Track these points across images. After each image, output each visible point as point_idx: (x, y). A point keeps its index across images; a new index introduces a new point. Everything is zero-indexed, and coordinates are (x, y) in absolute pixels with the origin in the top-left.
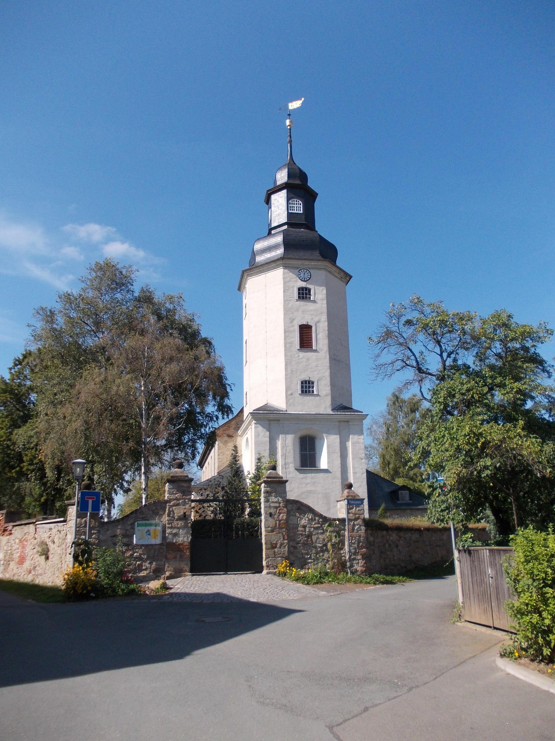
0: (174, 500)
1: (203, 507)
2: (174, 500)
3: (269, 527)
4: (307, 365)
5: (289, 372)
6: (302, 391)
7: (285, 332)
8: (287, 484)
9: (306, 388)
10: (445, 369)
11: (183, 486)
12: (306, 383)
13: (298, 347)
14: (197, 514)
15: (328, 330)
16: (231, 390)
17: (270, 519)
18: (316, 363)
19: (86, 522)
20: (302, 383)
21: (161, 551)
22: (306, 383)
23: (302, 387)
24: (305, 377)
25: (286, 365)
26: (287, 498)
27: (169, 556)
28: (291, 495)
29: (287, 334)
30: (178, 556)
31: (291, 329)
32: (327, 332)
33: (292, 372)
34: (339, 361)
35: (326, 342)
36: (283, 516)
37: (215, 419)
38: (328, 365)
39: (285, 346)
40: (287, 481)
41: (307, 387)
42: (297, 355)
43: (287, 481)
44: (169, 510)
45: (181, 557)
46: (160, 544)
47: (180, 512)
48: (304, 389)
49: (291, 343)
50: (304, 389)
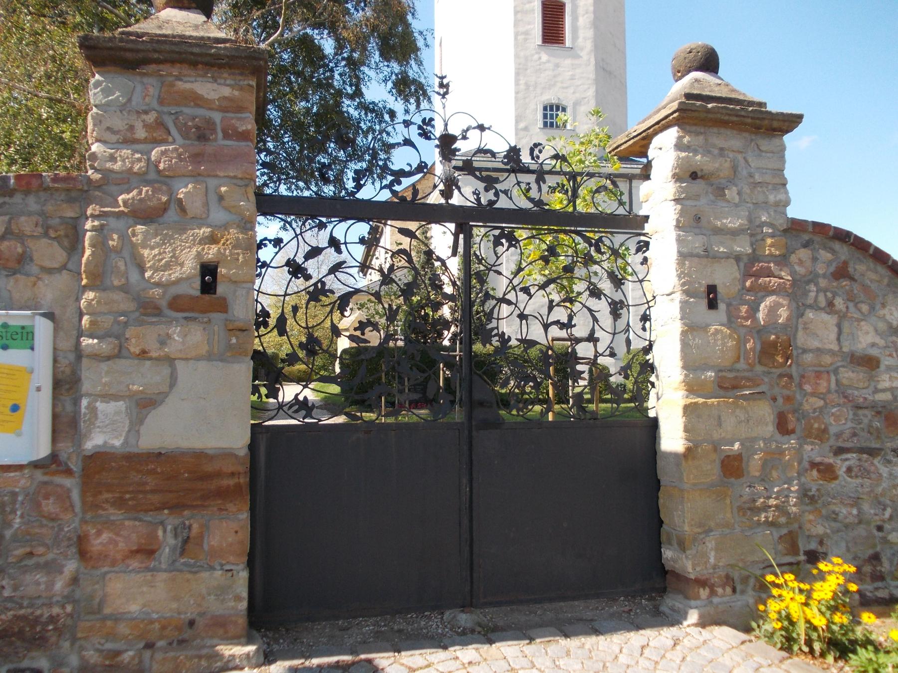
0: (142, 178)
1: (334, 243)
2: (142, 178)
3: (706, 367)
4: (555, 76)
5: (522, 87)
6: (545, 124)
7: (516, 13)
8: (794, 142)
9: (552, 117)
10: (30, 598)
11: (197, 100)
12: (552, 110)
13: (539, 41)
14: (299, 284)
15: (595, 12)
16: (427, 46)
17: (716, 323)
18: (570, 73)
19: (573, 390)
20: (545, 109)
21: (50, 506)
22: (552, 110)
23: (545, 116)
24: (550, 97)
25: (517, 74)
26: (794, 212)
27: (99, 542)
28: (810, 198)
29: (519, 16)
30: (168, 541)
31: (527, 6)
32: (592, 16)
33: (527, 85)
34: (610, 73)
35: (590, 33)
36: (773, 310)
37: (387, 117)
38: (592, 76)
39: (516, 39)
40: (791, 121)
41: (552, 114)
42: (536, 57)
43: (791, 121)
44: (100, 244)
45: (186, 544)
46: (36, 465)
47: (175, 261)
48: (549, 120)
49: (526, 33)
50: (549, 120)
